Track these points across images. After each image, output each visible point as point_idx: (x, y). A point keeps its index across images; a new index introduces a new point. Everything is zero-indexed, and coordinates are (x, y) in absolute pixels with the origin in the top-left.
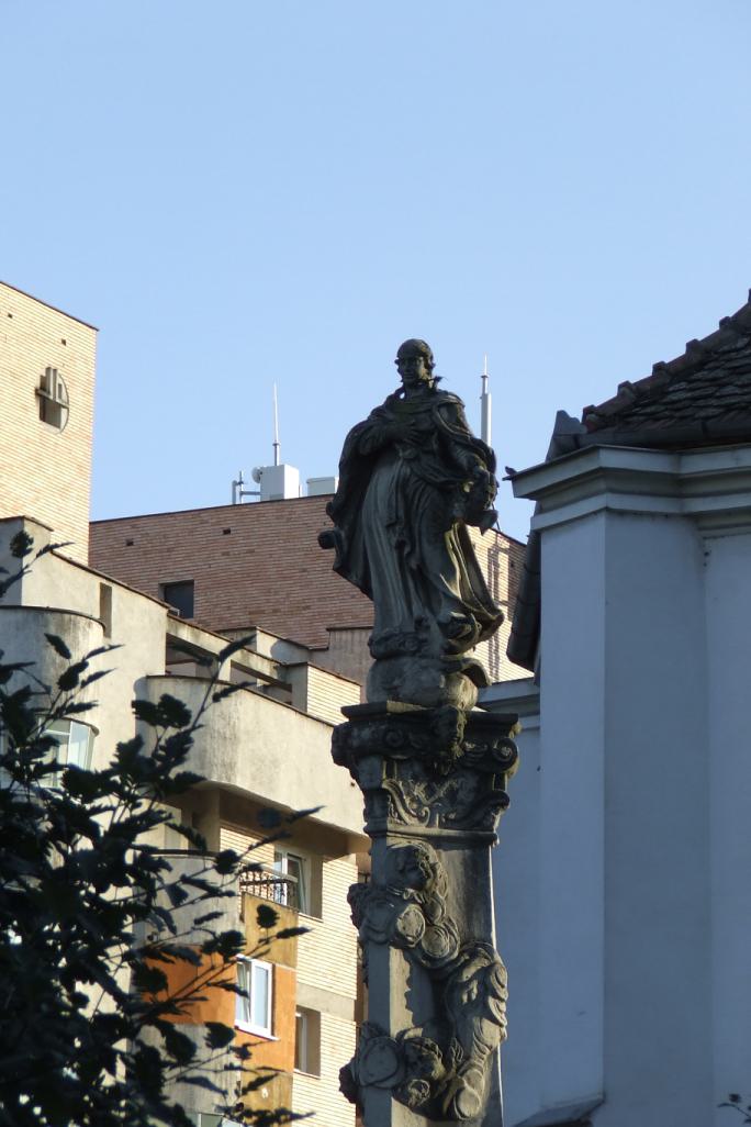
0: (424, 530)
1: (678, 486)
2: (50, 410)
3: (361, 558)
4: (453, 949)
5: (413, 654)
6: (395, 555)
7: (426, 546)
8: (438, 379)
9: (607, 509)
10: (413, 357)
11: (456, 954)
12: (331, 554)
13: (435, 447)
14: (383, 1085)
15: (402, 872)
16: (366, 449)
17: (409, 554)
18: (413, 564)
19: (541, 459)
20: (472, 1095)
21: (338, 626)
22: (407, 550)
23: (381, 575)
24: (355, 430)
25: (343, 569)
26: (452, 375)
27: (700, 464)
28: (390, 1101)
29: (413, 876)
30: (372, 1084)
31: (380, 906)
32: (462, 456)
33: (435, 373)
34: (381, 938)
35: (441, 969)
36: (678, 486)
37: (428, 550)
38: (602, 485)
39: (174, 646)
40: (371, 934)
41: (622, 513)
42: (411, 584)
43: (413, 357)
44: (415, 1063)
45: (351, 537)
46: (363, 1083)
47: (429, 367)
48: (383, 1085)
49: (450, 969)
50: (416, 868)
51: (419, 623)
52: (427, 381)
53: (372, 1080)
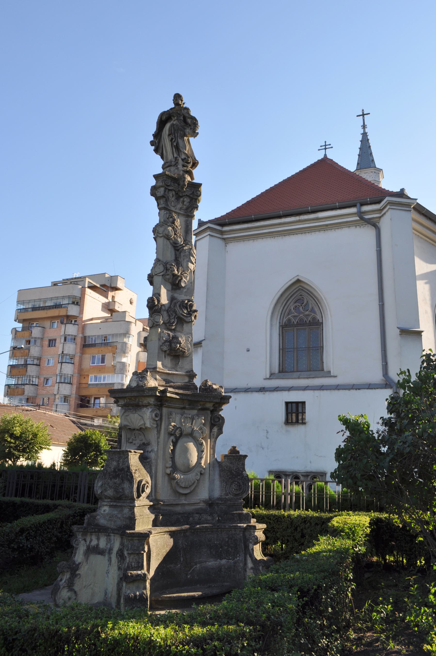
0: (178, 135)
1: (222, 233)
2: (131, 303)
3: (161, 149)
4: (181, 242)
5: (174, 166)
6: (170, 143)
7: (179, 139)
8: (184, 104)
9: (209, 234)
10: (177, 97)
11: (182, 243)
12: (153, 147)
13: (182, 119)
14: (159, 275)
15: (168, 218)
16: (164, 118)
17: (174, 141)
18: (175, 144)
19: (197, 228)
20: (185, 281)
21: (174, 503)
22: (174, 140)
23: (166, 152)
24: (161, 114)
25: (156, 151)
26: (187, 102)
27: (226, 228)
28: (160, 287)
29: (171, 219)
30: (156, 275)
31: (161, 227)
32: (189, 121)
33: (183, 102)
34: (161, 235)
35: (177, 247)
36: (222, 233)
37: (180, 141)
38: (208, 230)
39: (144, 328)
40: (158, 234)
41: (212, 236)
42: (174, 149)
43: (177, 97)
44: (169, 269)
45: (159, 142)
46: (154, 274)
47: (182, 100)
48: (159, 275)
49: (180, 247)
50: (172, 217)
51: (176, 158)
52: (181, 105)
53: (156, 273)
